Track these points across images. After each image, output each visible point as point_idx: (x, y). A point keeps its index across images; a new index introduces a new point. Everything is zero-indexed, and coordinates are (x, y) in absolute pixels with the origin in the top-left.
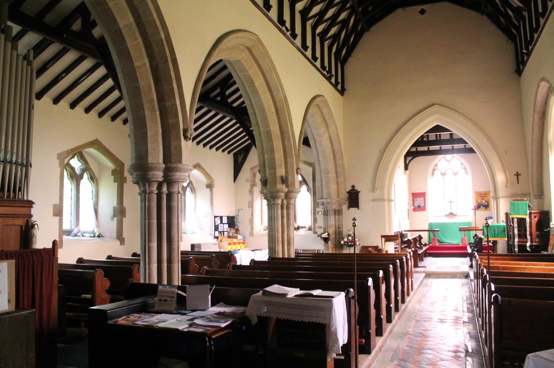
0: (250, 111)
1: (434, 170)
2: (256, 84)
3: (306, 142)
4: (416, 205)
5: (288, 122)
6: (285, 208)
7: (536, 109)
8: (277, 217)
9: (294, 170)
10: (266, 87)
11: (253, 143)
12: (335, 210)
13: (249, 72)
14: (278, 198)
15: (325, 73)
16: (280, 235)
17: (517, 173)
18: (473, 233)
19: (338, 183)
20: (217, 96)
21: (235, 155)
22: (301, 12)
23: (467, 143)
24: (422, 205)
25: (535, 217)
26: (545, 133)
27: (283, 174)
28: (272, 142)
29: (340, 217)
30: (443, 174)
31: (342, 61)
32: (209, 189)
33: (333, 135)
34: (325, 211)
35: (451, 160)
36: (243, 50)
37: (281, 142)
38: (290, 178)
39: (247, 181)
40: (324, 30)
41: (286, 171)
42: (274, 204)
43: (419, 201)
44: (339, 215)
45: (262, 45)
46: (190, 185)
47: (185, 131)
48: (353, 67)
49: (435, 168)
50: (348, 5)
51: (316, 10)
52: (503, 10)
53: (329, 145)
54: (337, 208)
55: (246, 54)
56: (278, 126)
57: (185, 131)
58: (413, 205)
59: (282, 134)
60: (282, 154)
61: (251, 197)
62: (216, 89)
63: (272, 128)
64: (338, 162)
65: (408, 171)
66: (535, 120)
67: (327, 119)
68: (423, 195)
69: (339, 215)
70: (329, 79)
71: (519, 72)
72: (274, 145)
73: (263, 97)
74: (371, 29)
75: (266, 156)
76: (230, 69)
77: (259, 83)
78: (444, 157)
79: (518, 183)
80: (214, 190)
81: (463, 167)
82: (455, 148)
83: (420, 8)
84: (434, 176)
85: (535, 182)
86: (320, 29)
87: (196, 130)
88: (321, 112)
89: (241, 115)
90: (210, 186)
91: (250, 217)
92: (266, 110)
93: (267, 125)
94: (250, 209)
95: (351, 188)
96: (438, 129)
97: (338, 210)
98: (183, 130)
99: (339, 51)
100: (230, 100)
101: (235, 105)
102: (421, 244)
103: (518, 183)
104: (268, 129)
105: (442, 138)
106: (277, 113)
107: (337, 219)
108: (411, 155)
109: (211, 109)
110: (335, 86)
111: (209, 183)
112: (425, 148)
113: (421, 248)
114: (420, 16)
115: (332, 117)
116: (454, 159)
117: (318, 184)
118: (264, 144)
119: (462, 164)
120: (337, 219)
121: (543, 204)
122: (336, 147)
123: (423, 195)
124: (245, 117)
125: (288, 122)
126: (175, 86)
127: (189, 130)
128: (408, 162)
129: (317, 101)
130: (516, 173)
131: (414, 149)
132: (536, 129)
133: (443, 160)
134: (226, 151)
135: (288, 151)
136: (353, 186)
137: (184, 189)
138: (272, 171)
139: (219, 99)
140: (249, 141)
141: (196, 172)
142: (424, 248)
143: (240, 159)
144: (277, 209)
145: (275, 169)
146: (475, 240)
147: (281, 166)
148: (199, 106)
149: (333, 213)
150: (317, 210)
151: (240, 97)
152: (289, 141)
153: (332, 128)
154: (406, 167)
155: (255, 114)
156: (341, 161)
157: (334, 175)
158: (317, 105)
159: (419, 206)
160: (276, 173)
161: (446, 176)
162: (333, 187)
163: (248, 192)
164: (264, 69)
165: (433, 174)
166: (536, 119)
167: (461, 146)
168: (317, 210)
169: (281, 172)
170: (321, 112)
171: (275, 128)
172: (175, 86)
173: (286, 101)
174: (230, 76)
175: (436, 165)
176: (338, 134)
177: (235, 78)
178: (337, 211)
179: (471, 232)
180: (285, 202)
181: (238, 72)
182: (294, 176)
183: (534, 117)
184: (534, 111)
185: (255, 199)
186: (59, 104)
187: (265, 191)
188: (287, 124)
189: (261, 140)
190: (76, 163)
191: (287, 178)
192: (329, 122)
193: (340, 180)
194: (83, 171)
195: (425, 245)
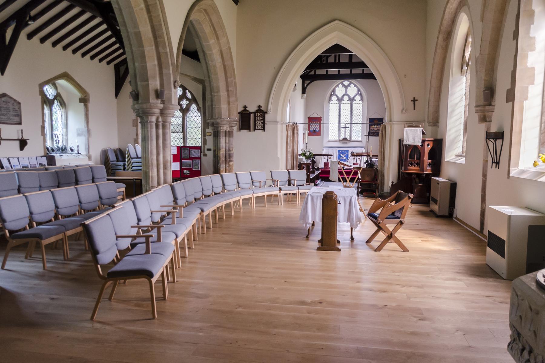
0: (114, 6)
1: (331, 95)
3: (191, 53)
4: (312, 129)
5: (162, 23)
6: (161, 127)
7: (442, 27)
8: (151, 137)
12: (225, 131)
14: (153, 114)
16: (155, 157)
17: (414, 98)
18: (365, 159)
19: (229, 103)
21: (117, 67)
23: (368, 67)
24: (318, 130)
25: (428, 145)
26: (447, 57)
27: (158, 87)
28: (143, 47)
29: (231, 138)
30: (340, 100)
32: (82, 104)
33: (224, 49)
35: (349, 85)
37: (154, 47)
38: (166, 92)
41: (162, 85)
42: (147, 122)
43: (314, 126)
44: (229, 137)
46: (58, 98)
54: (228, 129)
56: (149, 27)
58: (309, 130)
59: (155, 37)
60: (156, 63)
63: (141, 29)
64: (229, 79)
65: (305, 95)
66: (439, 42)
67: (217, 29)
68: (318, 120)
69: (229, 137)
72: (146, 51)
75: (137, 64)
78: (342, 83)
79: (414, 109)
80: (90, 105)
84: (331, 102)
85: (431, 109)
88: (210, 20)
90: (84, 100)
91: (135, 137)
92: (133, 5)
93: (136, 25)
94: (135, 128)
95: (242, 109)
96: (337, 48)
102: (313, 168)
103: (414, 109)
104: (137, 30)
105: (341, 61)
106: (149, 11)
107: (227, 141)
108: (308, 77)
109: (74, 4)
111: (83, 97)
112: (322, 72)
113: (314, 173)
115: (223, 28)
116: (352, 85)
117: (208, 103)
119: (359, 90)
120: (227, 141)
121: (436, 132)
122: (228, 63)
123: (318, 120)
124: (111, 14)
125: (162, 23)
128: (305, 85)
130: (413, 99)
132: (439, 51)
133: (340, 86)
134: (105, 62)
135: (163, 60)
136: (245, 107)
138: (144, 83)
142: (317, 173)
144: (151, 128)
145: (147, 80)
146: (367, 166)
147: (154, 77)
149: (224, 134)
150: (207, 130)
152: (164, 47)
153: (223, 40)
154: (304, 92)
156: (232, 79)
157: (226, 93)
159: (314, 131)
160: (148, 85)
161: (354, 102)
165: (330, 99)
166: (441, 38)
167: (357, 71)
168: (207, 130)
169: (155, 84)
170: (210, 20)
171: (145, 30)
175: (334, 91)
176: (229, 48)
178: (227, 133)
182: (170, 90)
183: (438, 38)
184: (440, 31)
186: (56, 47)
187: (136, 106)
188: (161, 25)
189: (130, 44)
190: (50, 91)
191: (162, 92)
192: (219, 32)
193: (231, 99)
194: (55, 98)
195: (318, 169)
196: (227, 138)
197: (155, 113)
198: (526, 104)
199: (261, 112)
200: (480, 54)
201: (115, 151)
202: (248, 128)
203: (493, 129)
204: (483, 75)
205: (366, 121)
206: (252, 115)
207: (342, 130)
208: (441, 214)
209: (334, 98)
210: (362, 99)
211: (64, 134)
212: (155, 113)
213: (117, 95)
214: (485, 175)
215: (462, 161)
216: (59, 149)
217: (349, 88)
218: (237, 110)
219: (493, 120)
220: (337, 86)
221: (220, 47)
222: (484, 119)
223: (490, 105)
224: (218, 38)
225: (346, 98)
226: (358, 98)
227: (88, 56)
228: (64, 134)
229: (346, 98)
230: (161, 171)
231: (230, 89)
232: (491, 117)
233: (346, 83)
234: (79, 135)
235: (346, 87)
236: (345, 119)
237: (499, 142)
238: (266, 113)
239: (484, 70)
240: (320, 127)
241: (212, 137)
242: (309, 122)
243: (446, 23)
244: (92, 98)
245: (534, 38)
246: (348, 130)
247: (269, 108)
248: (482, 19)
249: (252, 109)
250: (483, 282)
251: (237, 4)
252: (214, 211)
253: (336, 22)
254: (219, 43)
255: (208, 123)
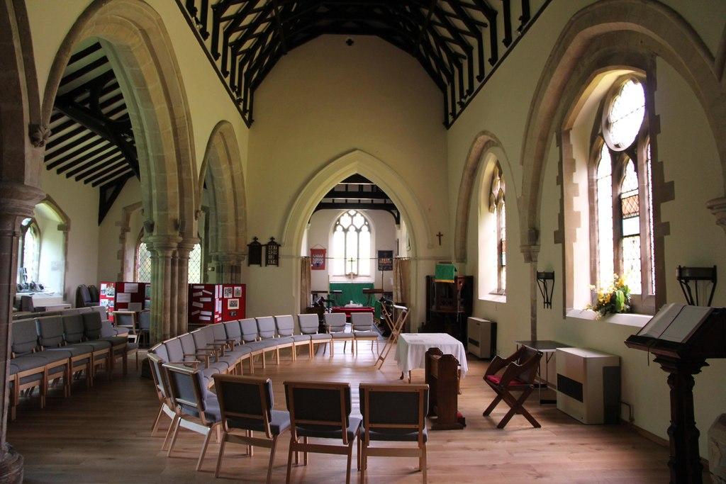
1: (336, 225)
2: (150, 87)
9: (192, 214)
10: (163, 95)
11: (136, 171)
13: (142, 68)
15: (234, 94)
19: (237, 234)
20: (85, 101)
21: (103, 190)
22: (213, 7)
23: (388, 198)
24: (321, 263)
25: (460, 283)
27: (178, 216)
30: (346, 231)
31: (253, 86)
32: (61, 232)
34: (218, 268)
35: (355, 215)
36: (136, 33)
38: (187, 223)
39: (117, 224)
40: (237, 41)
41: (182, 215)
45: (165, 32)
47: (34, 129)
48: (265, 94)
49: (367, 223)
50: (269, 16)
51: (232, 10)
52: (442, 51)
53: (230, 187)
54: (235, 264)
55: (140, 41)
57: (34, 129)
61: (121, 245)
62: (83, 92)
63: (166, 153)
64: (238, 207)
70: (237, 103)
71: (447, 125)
73: (157, 108)
74: (289, 53)
75: (154, 192)
76: (112, 64)
77: (154, 87)
78: (347, 212)
80: (70, 233)
81: (367, 223)
82: (335, 202)
83: (348, 37)
84: (336, 232)
86: (232, 38)
87: (54, 131)
88: (225, 143)
89: (119, 131)
90: (64, 228)
91: (120, 272)
95: (253, 241)
96: (357, 178)
97: (236, 266)
98: (30, 127)
99: (250, 73)
100: (105, 111)
101: (114, 117)
109: (74, 119)
110: (243, 113)
114: (346, 46)
116: (358, 215)
117: (211, 234)
118: (153, 174)
119: (366, 220)
120: (234, 278)
126: (17, 44)
127: (42, 128)
129: (223, 126)
131: (330, 200)
132: (465, 187)
133: (346, 215)
134: (90, 183)
137: (24, 229)
139: (87, 106)
140: (130, 169)
141: (44, 208)
143: (110, 192)
148: (56, 112)
150: (209, 265)
151: (124, 107)
153: (236, 166)
155: (143, 131)
158: (221, 133)
161: (348, 233)
162: (232, 238)
163: (117, 239)
164: (163, 68)
165: (335, 230)
166: (466, 174)
167: (381, 201)
170: (225, 143)
172: (17, 44)
173: (189, 119)
174: (110, 74)
175: (339, 220)
176: (242, 173)
177: (119, 78)
179: (375, 294)
180: (177, 255)
181: (124, 66)
185: (126, 248)
189: (149, 168)
191: (183, 223)
196: (234, 274)
197: (172, 248)
198: (575, 245)
199: (274, 244)
200: (522, 195)
201: (89, 289)
202: (260, 263)
203: (541, 269)
204: (527, 215)
205: (375, 255)
206: (264, 249)
207: (349, 264)
208: (484, 357)
209: (339, 228)
210: (369, 230)
211: (34, 268)
212: (172, 248)
213: (100, 221)
214: (534, 315)
215: (503, 299)
216: (28, 286)
217: (354, 218)
218: (246, 242)
219: (538, 259)
220: (343, 215)
221: (232, 172)
222: (530, 257)
223: (535, 245)
224: (230, 163)
225: (352, 229)
226: (365, 229)
227: (73, 177)
228: (34, 268)
229: (352, 229)
230: (176, 315)
231: (239, 218)
232: (536, 257)
233: (352, 212)
234: (54, 269)
235: (352, 217)
236: (352, 254)
237: (549, 282)
238: (280, 245)
239: (527, 211)
240: (324, 261)
241: (215, 273)
242: (312, 254)
243: (471, 161)
244: (73, 225)
245: (577, 184)
246: (355, 264)
247: (283, 241)
248: (522, 163)
249: (264, 240)
250: (563, 430)
251: (249, 128)
252: (239, 363)
253: (357, 152)
254: (231, 168)
255: (211, 257)
